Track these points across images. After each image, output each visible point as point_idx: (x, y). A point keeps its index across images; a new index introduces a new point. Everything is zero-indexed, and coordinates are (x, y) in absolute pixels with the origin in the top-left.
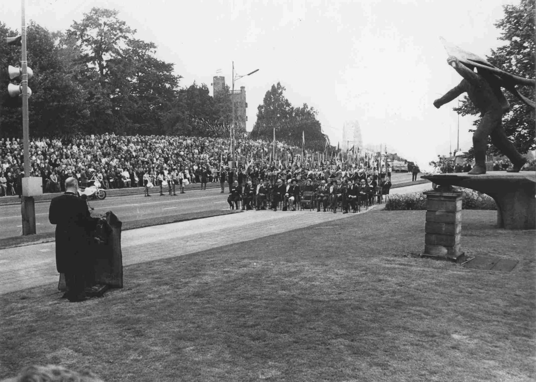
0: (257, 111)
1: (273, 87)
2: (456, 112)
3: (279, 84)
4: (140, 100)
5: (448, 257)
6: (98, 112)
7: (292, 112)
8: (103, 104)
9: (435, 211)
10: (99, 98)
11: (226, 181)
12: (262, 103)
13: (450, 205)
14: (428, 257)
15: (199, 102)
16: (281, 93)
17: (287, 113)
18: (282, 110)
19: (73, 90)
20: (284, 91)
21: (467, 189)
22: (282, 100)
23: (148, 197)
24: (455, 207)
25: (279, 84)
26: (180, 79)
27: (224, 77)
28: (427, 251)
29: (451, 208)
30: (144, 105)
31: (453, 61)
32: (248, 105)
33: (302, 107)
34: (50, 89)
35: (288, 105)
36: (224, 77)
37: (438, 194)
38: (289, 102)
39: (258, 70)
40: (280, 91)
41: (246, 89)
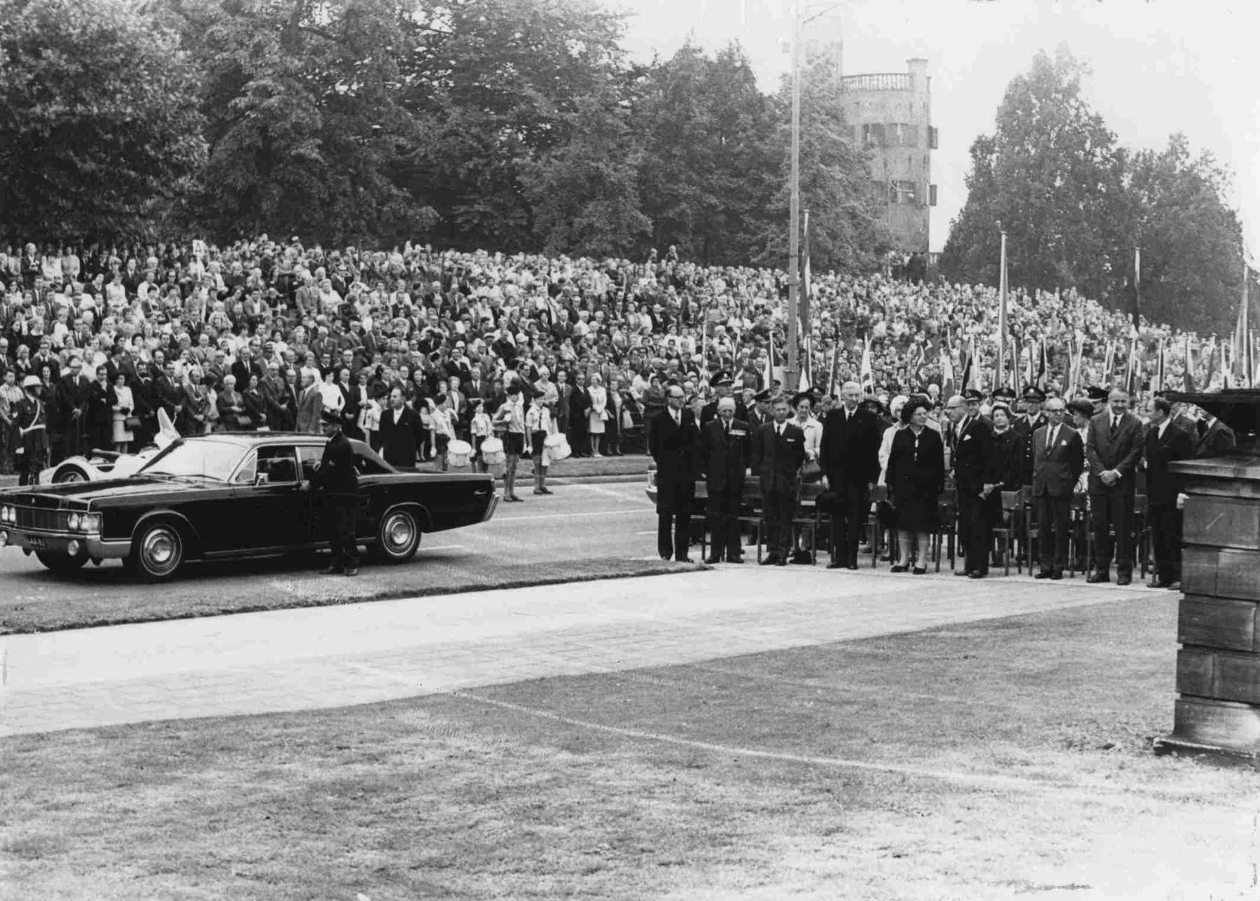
0: (967, 165)
4: (456, 102)
6: (266, 152)
7: (1118, 171)
8: (285, 117)
10: (265, 93)
11: (9, 373)
12: (990, 130)
14: (1182, 751)
15: (706, 118)
17: (1096, 175)
18: (1076, 160)
19: (133, 50)
22: (1078, 116)
23: (543, 497)
26: (628, 20)
28: (1182, 728)
30: (470, 124)
32: (942, 138)
33: (1161, 148)
34: (34, 47)
35: (1103, 138)
38: (1109, 126)
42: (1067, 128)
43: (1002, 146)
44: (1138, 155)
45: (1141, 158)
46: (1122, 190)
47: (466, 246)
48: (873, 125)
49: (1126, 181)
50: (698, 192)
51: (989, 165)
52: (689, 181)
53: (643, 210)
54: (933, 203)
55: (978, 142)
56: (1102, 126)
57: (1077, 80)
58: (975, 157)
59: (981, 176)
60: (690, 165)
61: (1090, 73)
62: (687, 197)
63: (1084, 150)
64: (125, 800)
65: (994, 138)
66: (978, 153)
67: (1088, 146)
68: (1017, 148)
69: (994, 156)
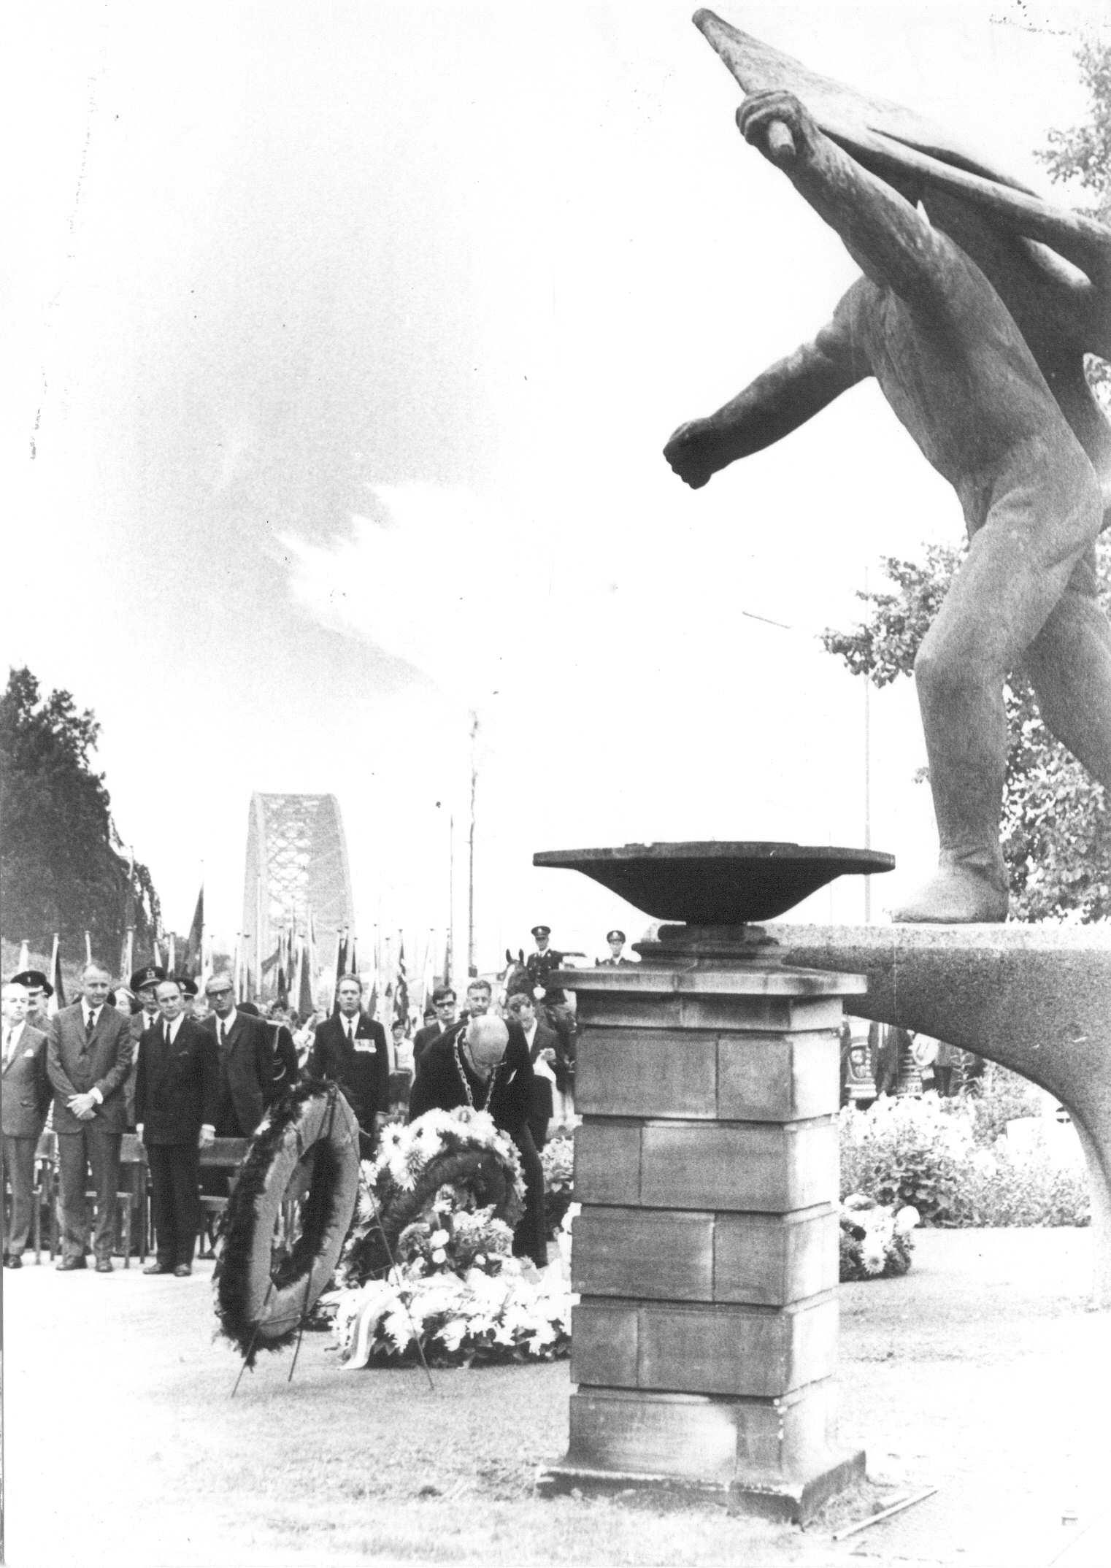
2: (841, 657)
5: (738, 1486)
9: (642, 1121)
13: (746, 1066)
14: (591, 1487)
24: (785, 1088)
29: (758, 1098)
31: (772, 117)
37: (659, 983)
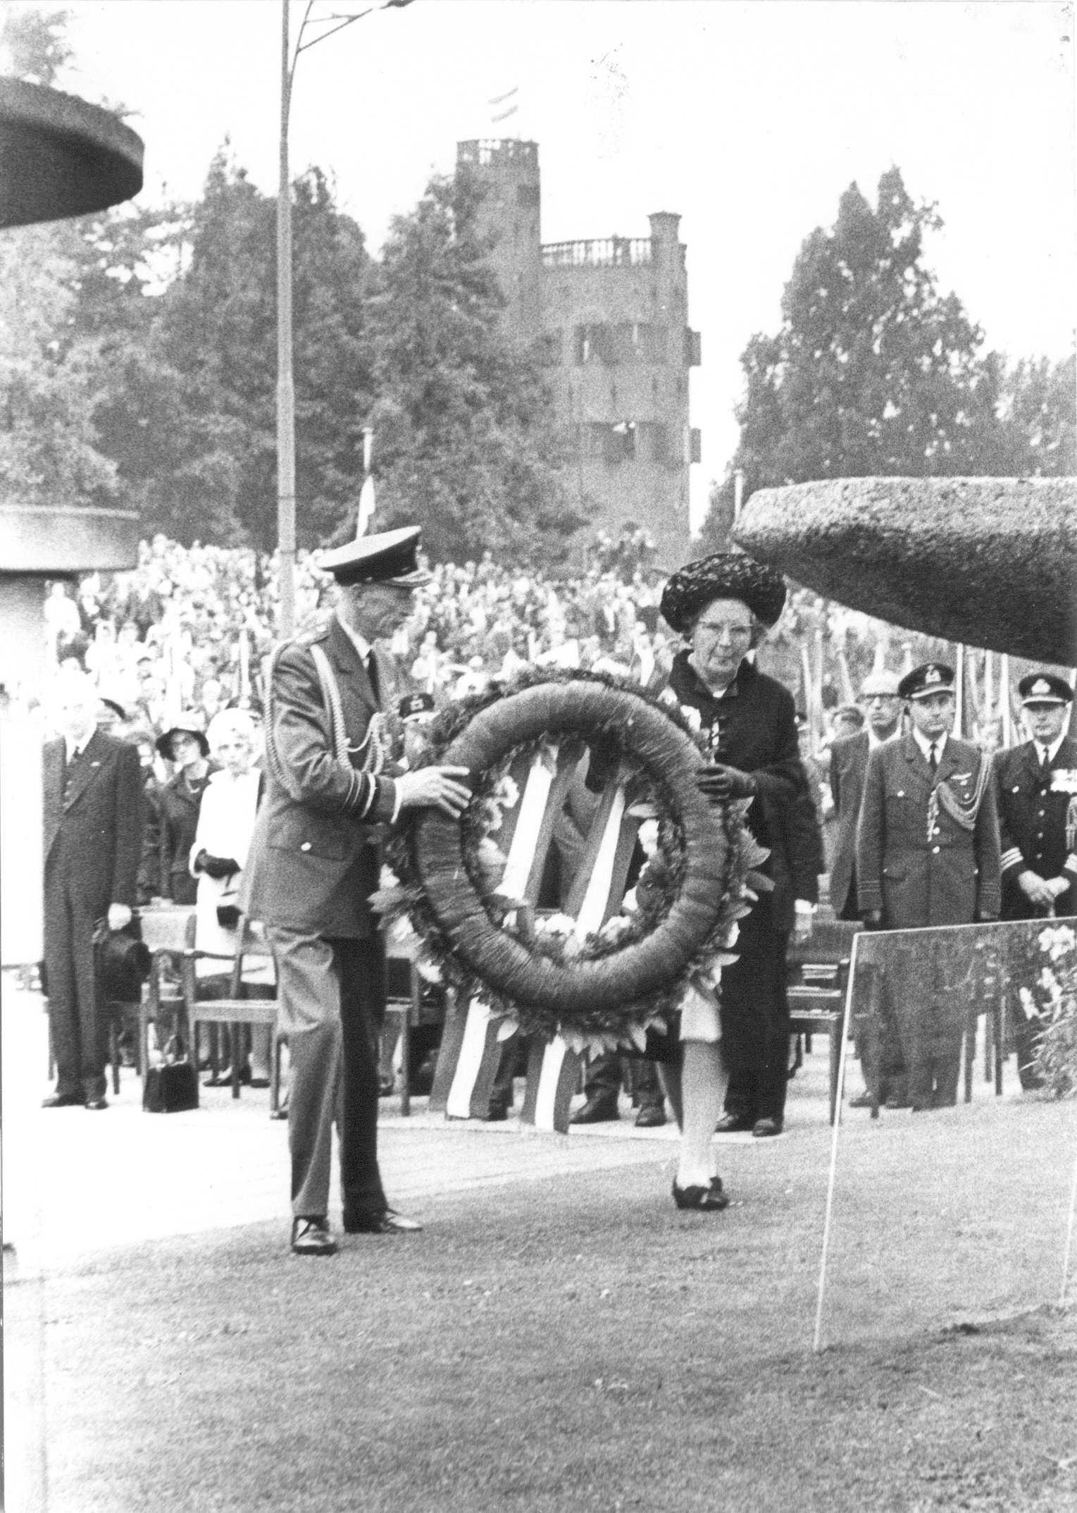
1: (852, 201)
3: (892, 182)
7: (988, 392)
16: (911, 251)
17: (960, 400)
20: (926, 232)
21: (112, 210)
25: (892, 182)
27: (533, 146)
33: (168, 208)
35: (965, 338)
36: (533, 146)
38: (971, 315)
39: (494, 120)
40: (899, 235)
41: (685, 234)
42: (900, 317)
43: (793, 352)
44: (1021, 364)
45: (1027, 369)
46: (995, 424)
47: (801, 784)
48: (594, 327)
49: (1004, 408)
50: (243, 427)
51: (771, 384)
52: (228, 410)
53: (100, 448)
54: (696, 458)
55: (751, 345)
56: (962, 315)
57: (916, 237)
58: (749, 369)
59: (758, 402)
60: (226, 382)
61: (939, 223)
62: (225, 436)
63: (931, 355)
64: (1021, 1310)
65: (779, 337)
66: (754, 363)
67: (937, 349)
68: (818, 354)
69: (780, 369)
